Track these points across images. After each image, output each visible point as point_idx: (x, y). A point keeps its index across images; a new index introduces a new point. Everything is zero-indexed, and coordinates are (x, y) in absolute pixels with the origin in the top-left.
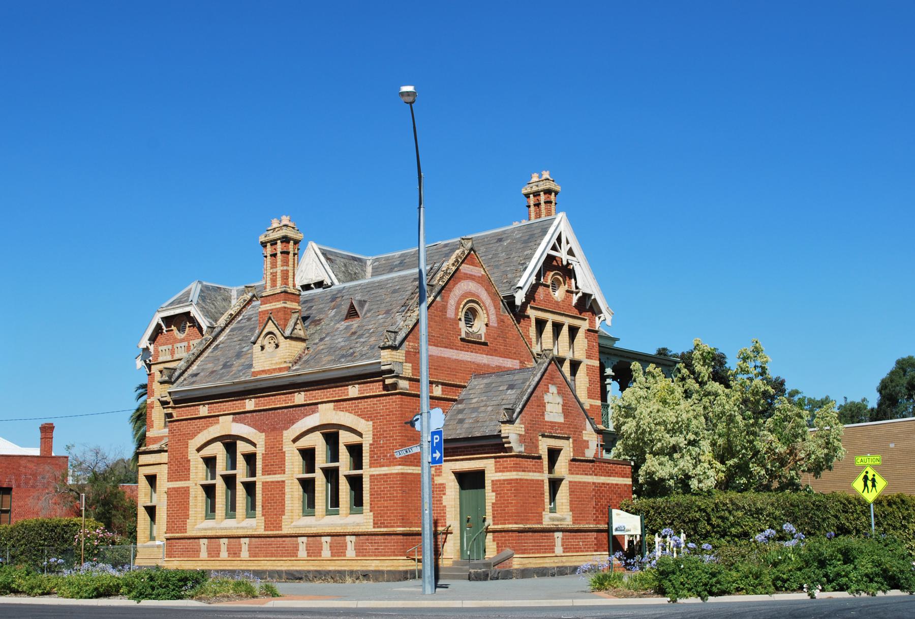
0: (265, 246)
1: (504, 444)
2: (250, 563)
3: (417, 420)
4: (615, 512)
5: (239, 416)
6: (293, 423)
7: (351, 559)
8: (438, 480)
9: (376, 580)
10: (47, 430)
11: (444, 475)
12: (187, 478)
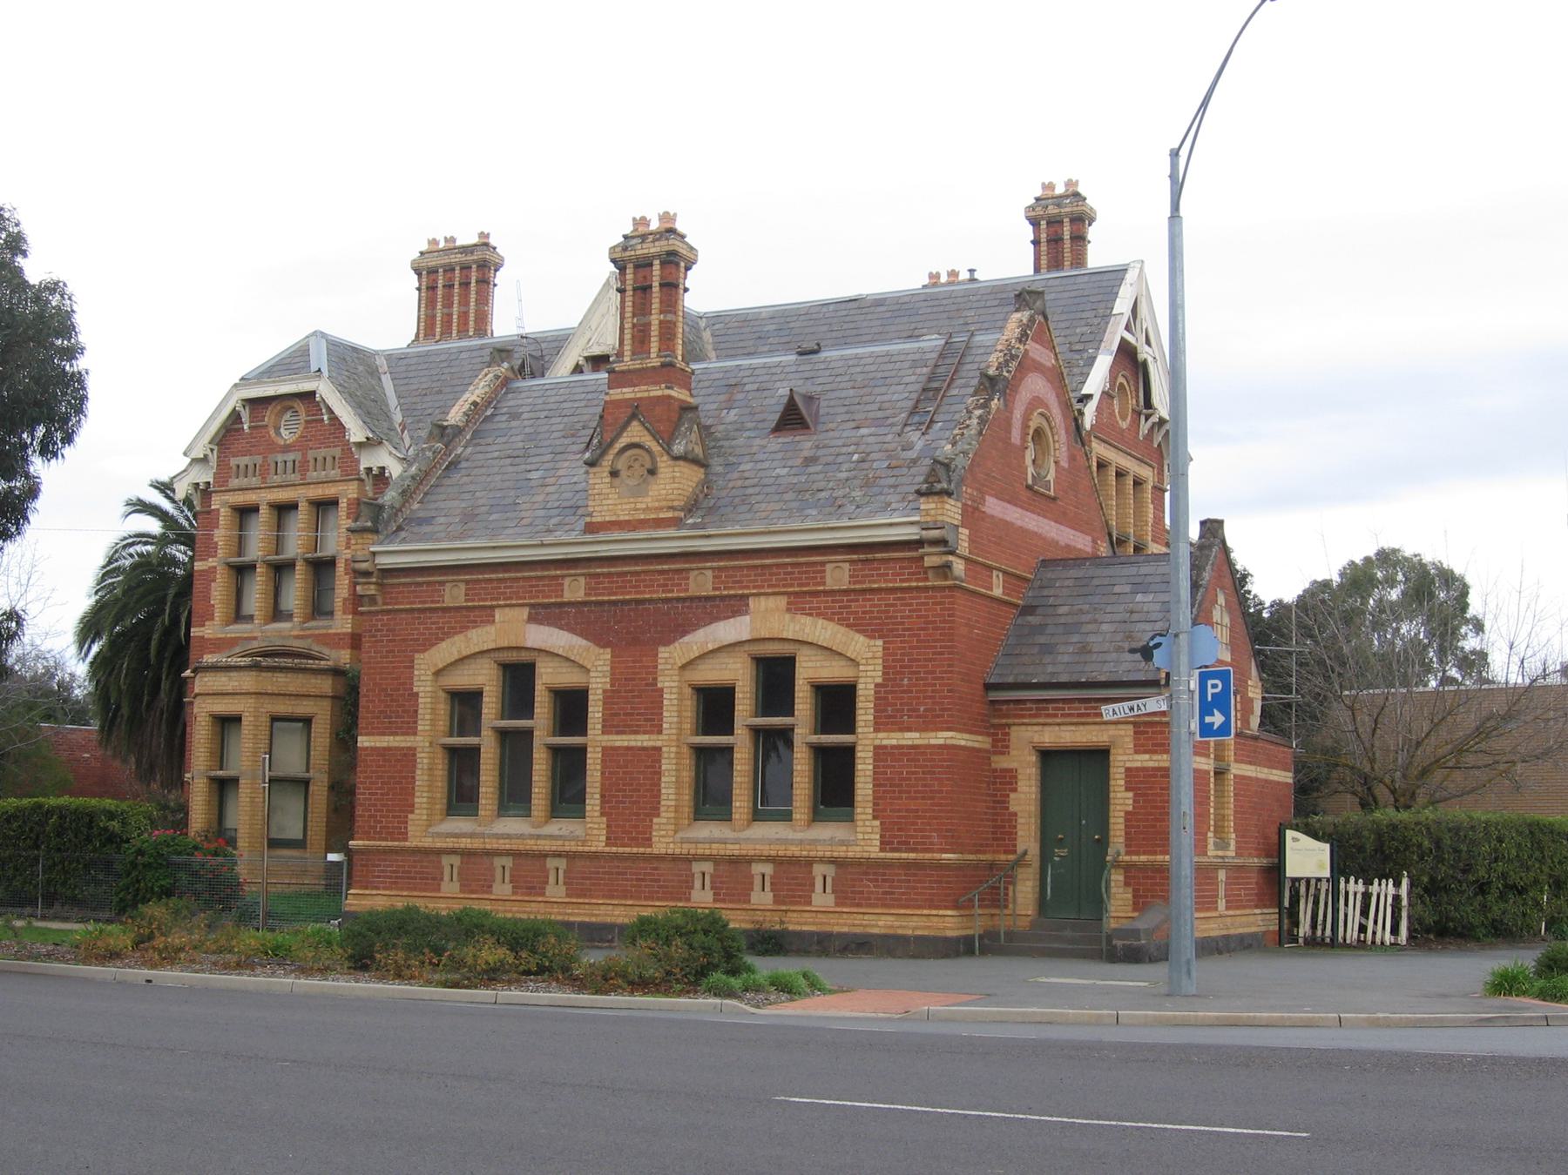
2: (833, 919)
3: (1158, 645)
4: (1290, 834)
6: (684, 633)
8: (1001, 762)
11: (1013, 753)
12: (413, 731)
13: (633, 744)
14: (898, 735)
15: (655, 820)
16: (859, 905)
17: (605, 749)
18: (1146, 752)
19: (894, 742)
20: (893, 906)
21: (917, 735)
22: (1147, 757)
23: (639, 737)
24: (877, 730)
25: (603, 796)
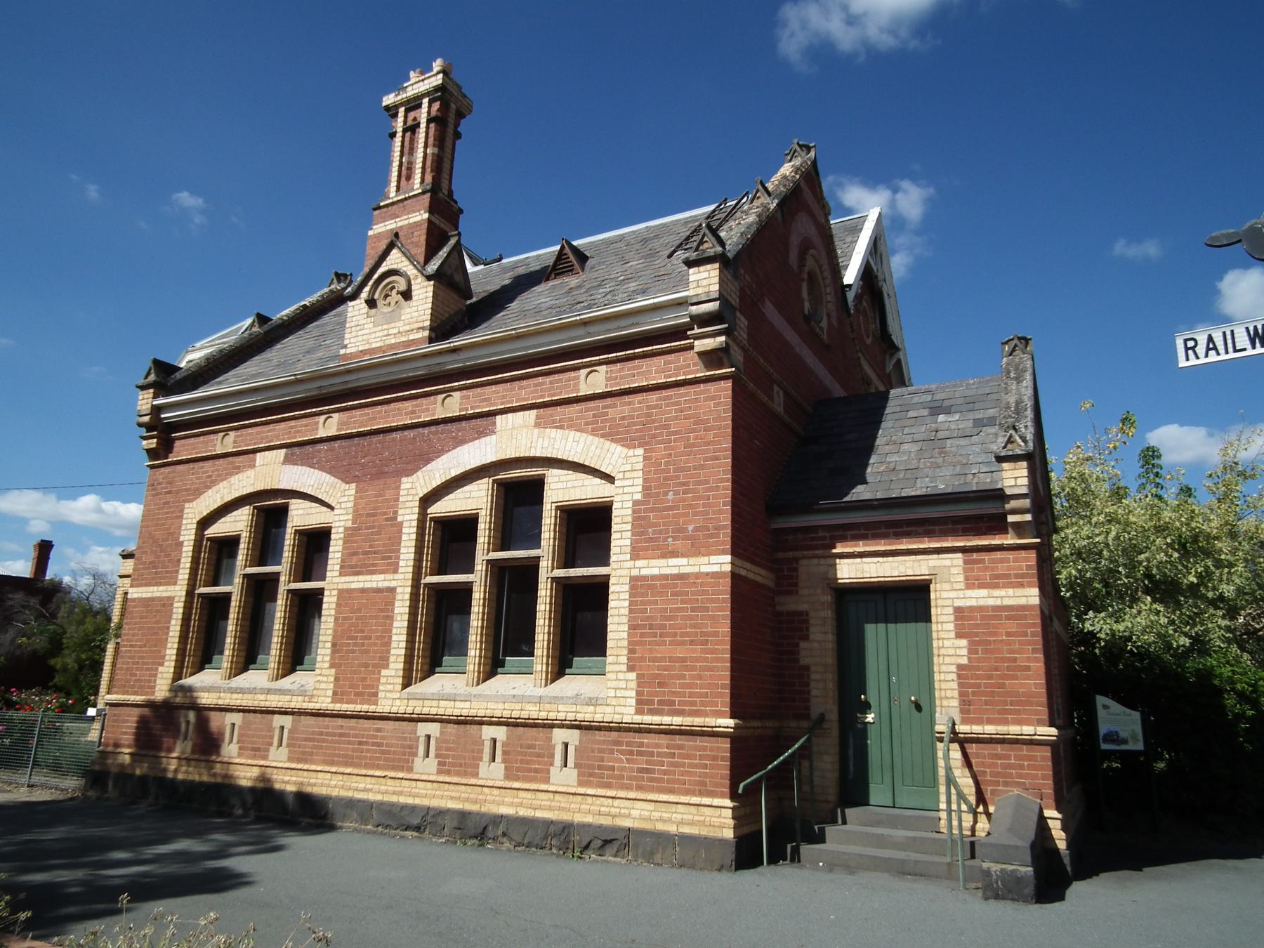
0: (395, 115)
1: (1004, 516)
5: (299, 451)
6: (428, 461)
7: (562, 796)
8: (790, 604)
9: (649, 857)
10: (44, 549)
11: (803, 592)
13: (368, 585)
14: (662, 562)
15: (384, 672)
16: (608, 786)
17: (341, 592)
18: (981, 586)
19: (656, 571)
20: (651, 790)
21: (684, 561)
22: (984, 592)
23: (374, 577)
24: (634, 557)
25: (334, 645)
